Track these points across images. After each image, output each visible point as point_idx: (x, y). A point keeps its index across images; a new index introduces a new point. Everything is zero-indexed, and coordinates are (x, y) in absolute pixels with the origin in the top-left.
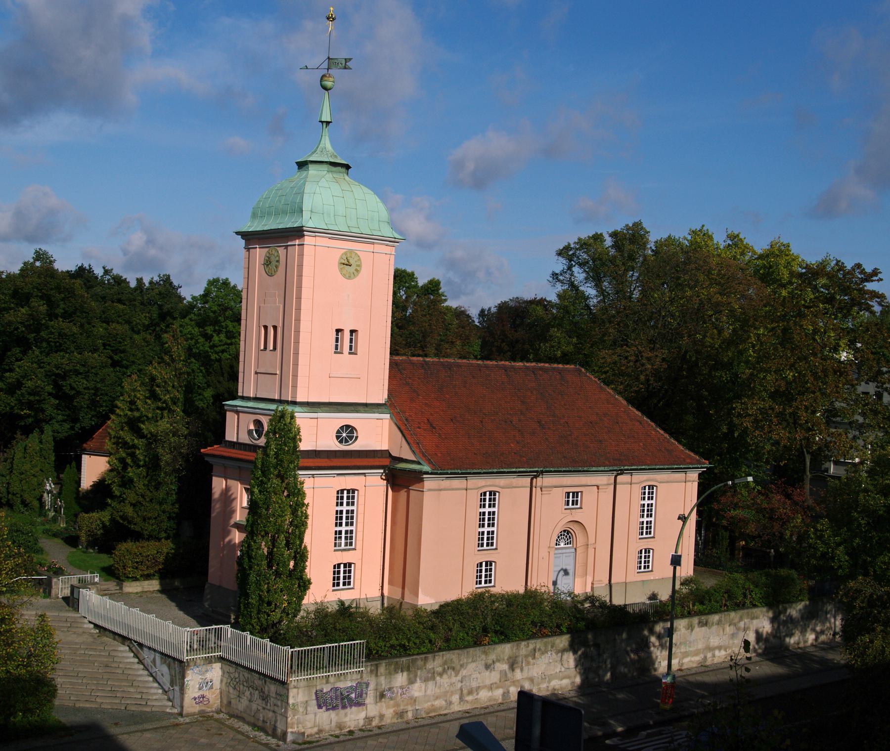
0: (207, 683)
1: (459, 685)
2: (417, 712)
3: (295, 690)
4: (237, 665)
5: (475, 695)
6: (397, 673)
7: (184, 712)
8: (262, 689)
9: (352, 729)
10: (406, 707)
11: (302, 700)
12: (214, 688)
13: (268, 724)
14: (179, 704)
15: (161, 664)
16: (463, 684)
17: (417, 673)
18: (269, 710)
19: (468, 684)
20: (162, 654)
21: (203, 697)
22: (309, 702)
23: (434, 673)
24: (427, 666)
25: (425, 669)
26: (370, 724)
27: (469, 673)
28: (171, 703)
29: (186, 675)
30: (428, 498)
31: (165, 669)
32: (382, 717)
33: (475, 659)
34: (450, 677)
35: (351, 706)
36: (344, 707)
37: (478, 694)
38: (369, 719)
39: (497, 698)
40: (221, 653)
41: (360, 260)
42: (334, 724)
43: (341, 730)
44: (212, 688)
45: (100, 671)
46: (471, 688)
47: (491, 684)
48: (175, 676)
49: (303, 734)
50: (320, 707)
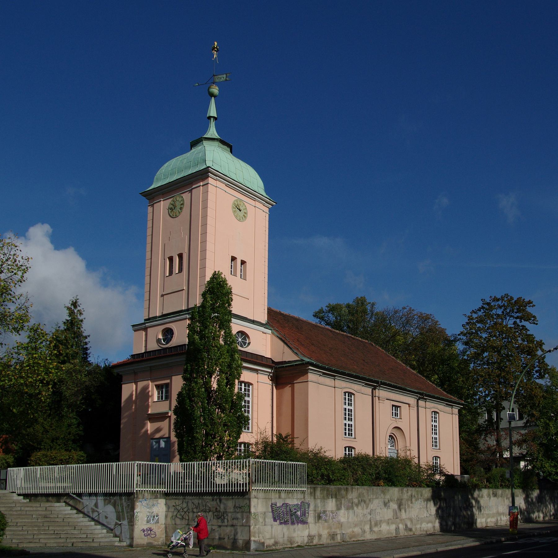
0: (154, 517)
1: (369, 517)
2: (343, 536)
3: (255, 500)
4: (184, 494)
5: (379, 527)
6: (329, 498)
7: (135, 543)
8: (216, 509)
9: (299, 544)
10: (336, 530)
11: (261, 511)
12: (160, 523)
13: (226, 540)
14: (128, 537)
15: (105, 505)
16: (372, 516)
17: (342, 501)
18: (227, 526)
19: (374, 517)
20: (105, 495)
21: (151, 530)
22: (266, 514)
23: (352, 503)
24: (348, 496)
25: (347, 498)
26: (312, 542)
27: (374, 508)
28: (118, 538)
29: (136, 507)
30: (311, 386)
31: (110, 509)
32: (320, 536)
33: (377, 496)
34: (363, 509)
35: (298, 523)
36: (293, 523)
37: (381, 527)
38: (311, 537)
39: (392, 532)
40: (166, 490)
41: (246, 209)
42: (286, 538)
43: (291, 544)
44: (158, 523)
45: (39, 521)
46: (377, 521)
47: (388, 520)
48: (123, 511)
49: (263, 543)
50: (275, 520)
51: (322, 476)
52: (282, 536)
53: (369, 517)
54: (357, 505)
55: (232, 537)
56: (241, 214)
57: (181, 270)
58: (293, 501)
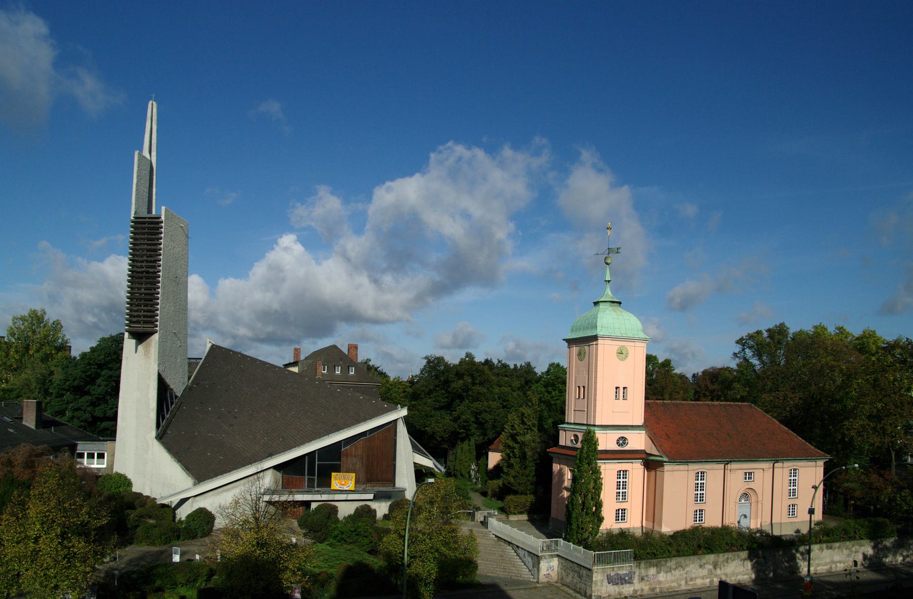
1: (685, 575)
3: (596, 574)
4: (566, 559)
20: (528, 552)
26: (636, 594)
31: (530, 559)
35: (626, 584)
36: (622, 584)
37: (695, 581)
41: (628, 351)
42: (616, 592)
43: (621, 595)
49: (600, 596)
50: (609, 583)
51: (648, 553)
52: (614, 591)
53: (685, 575)
54: (675, 570)
55: (585, 590)
56: (623, 356)
57: (584, 398)
58: (622, 572)
